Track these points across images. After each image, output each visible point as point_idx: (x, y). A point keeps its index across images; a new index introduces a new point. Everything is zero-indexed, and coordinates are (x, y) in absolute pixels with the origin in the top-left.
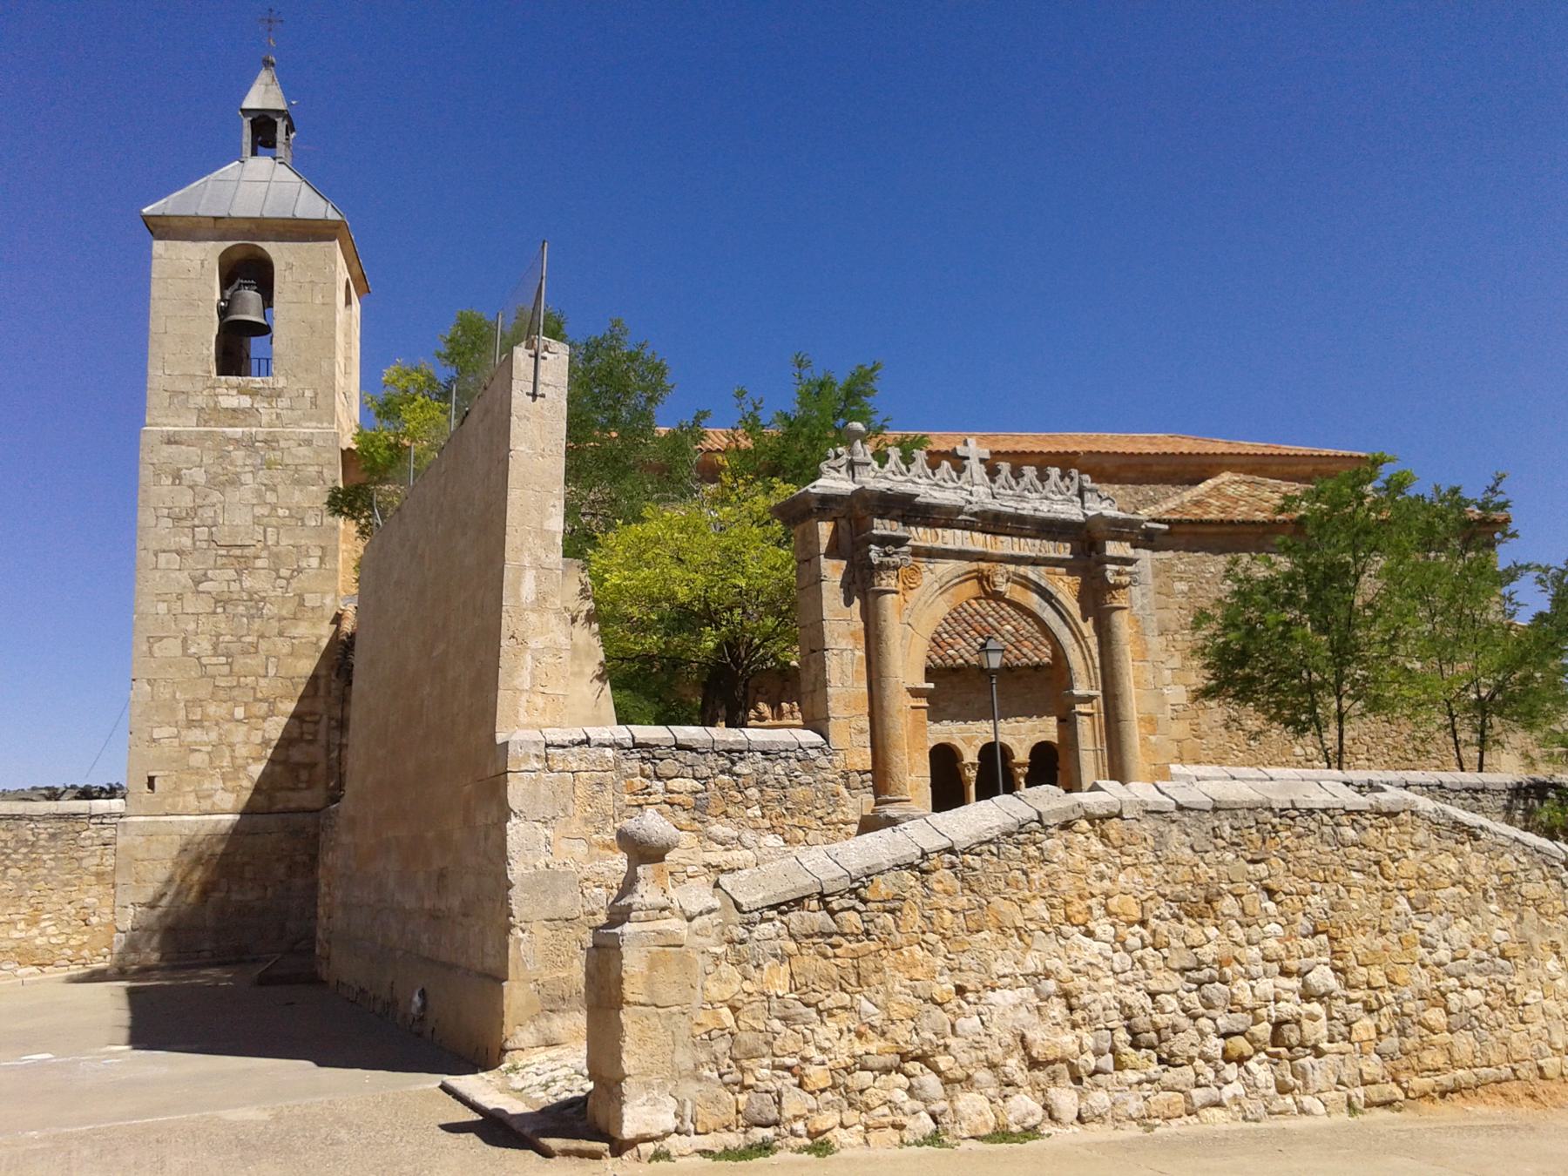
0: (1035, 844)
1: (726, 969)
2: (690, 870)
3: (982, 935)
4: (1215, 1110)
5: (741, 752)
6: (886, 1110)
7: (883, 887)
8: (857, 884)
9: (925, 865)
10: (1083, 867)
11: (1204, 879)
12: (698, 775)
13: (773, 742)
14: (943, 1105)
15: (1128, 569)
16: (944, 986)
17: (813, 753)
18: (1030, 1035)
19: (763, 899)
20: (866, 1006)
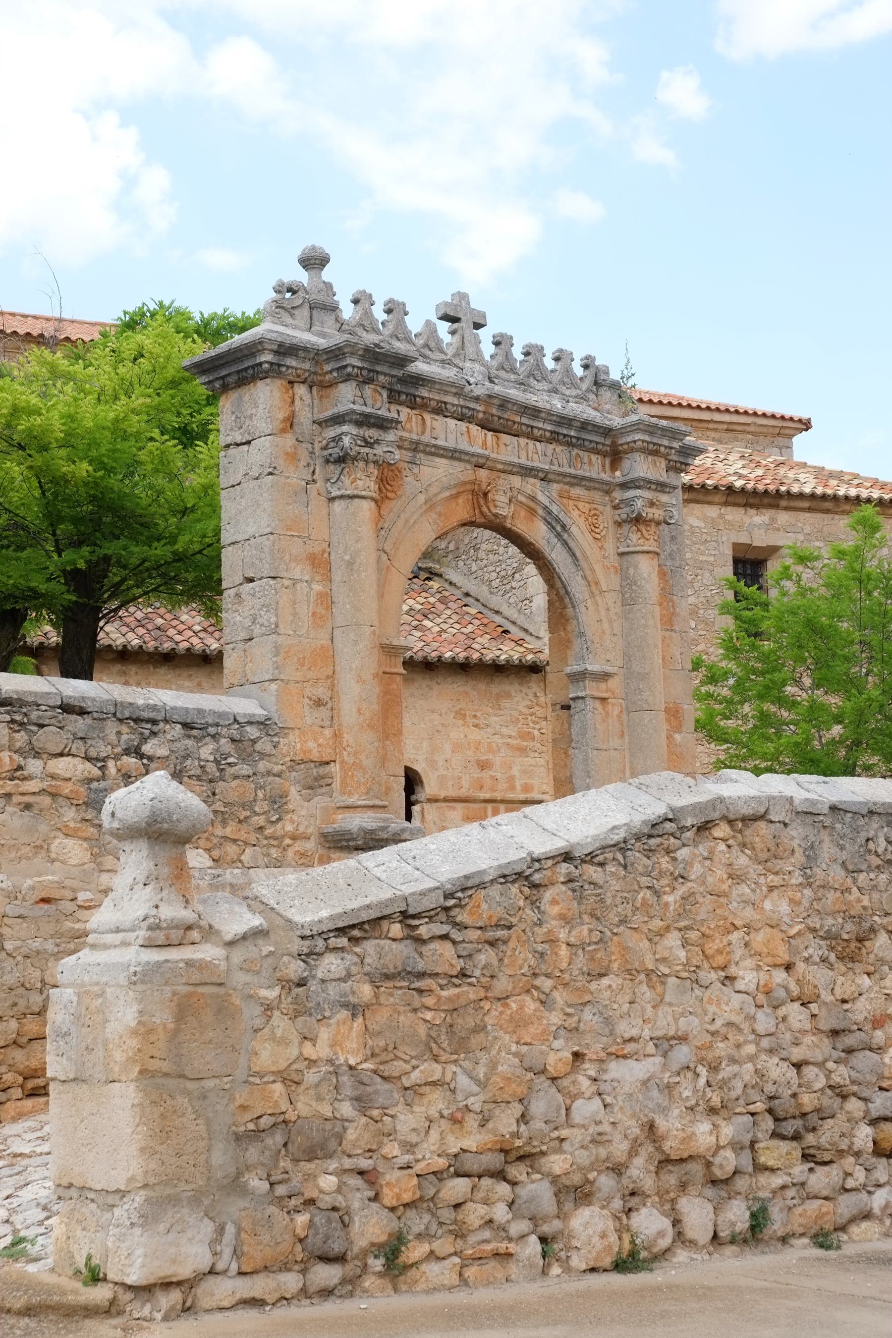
0: (668, 852)
1: (280, 1023)
2: (82, 896)
3: (605, 981)
4: (865, 1225)
5: (154, 722)
6: (487, 1234)
7: (488, 906)
8: (451, 902)
9: (537, 878)
10: (725, 887)
11: (856, 910)
12: (93, 753)
13: (200, 711)
14: (557, 1224)
15: (664, 498)
16: (557, 1056)
17: (252, 732)
18: (662, 1124)
19: (331, 918)
20: (463, 1081)
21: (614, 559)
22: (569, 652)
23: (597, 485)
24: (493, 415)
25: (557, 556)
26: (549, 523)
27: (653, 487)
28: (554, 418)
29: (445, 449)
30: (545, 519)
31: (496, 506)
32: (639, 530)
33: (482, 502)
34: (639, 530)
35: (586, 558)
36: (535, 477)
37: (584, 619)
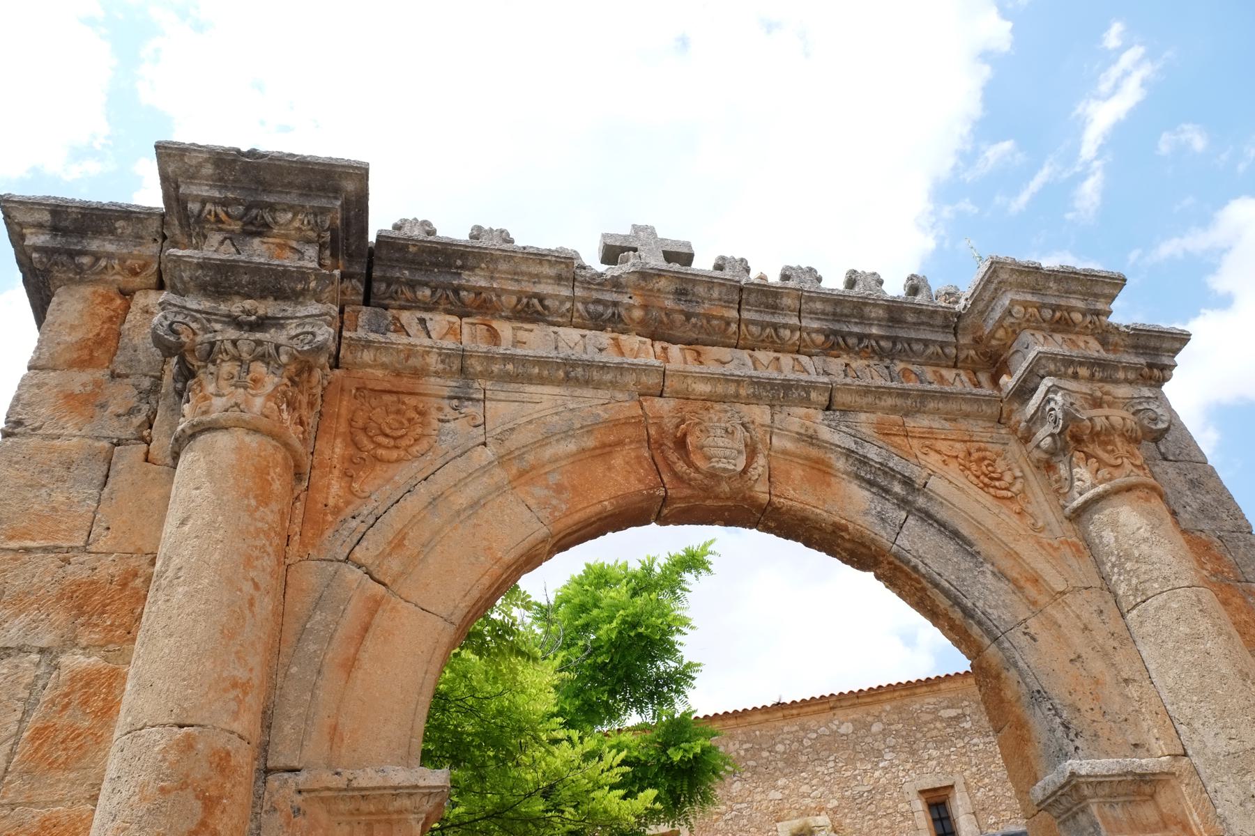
21: (1060, 530)
22: (1030, 751)
23: (966, 407)
24: (668, 313)
25: (916, 542)
26: (871, 483)
27: (1084, 372)
28: (819, 306)
29: (540, 362)
30: (858, 477)
31: (709, 459)
32: (1088, 456)
33: (673, 456)
34: (1088, 456)
35: (989, 535)
36: (806, 402)
37: (1032, 660)
